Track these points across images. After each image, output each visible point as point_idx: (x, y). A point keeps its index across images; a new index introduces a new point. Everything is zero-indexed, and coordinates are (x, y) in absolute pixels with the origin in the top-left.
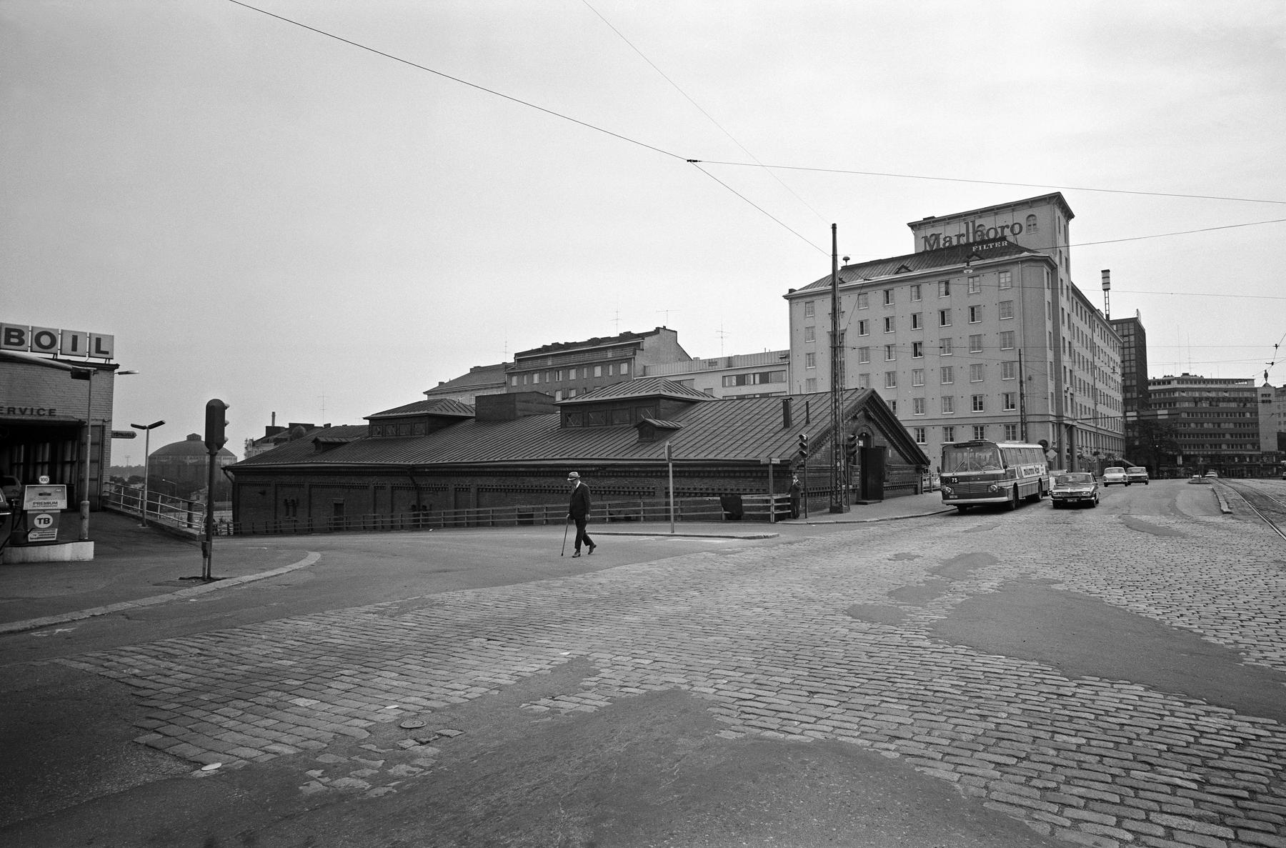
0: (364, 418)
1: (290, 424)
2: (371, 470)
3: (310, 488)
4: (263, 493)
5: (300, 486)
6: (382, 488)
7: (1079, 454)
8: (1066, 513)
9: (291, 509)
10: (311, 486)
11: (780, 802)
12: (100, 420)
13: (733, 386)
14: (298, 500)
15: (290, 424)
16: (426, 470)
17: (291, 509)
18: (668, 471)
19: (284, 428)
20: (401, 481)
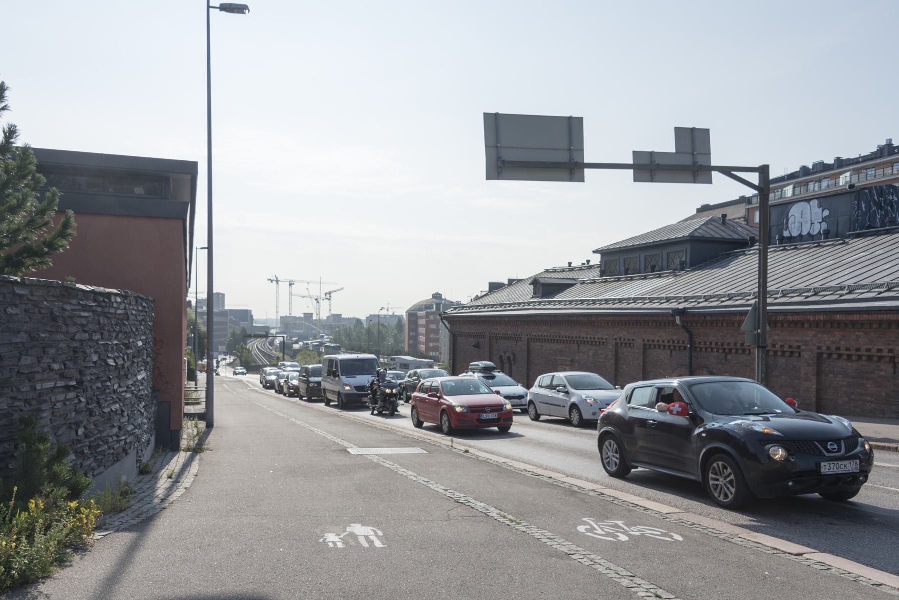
0: (594, 252)
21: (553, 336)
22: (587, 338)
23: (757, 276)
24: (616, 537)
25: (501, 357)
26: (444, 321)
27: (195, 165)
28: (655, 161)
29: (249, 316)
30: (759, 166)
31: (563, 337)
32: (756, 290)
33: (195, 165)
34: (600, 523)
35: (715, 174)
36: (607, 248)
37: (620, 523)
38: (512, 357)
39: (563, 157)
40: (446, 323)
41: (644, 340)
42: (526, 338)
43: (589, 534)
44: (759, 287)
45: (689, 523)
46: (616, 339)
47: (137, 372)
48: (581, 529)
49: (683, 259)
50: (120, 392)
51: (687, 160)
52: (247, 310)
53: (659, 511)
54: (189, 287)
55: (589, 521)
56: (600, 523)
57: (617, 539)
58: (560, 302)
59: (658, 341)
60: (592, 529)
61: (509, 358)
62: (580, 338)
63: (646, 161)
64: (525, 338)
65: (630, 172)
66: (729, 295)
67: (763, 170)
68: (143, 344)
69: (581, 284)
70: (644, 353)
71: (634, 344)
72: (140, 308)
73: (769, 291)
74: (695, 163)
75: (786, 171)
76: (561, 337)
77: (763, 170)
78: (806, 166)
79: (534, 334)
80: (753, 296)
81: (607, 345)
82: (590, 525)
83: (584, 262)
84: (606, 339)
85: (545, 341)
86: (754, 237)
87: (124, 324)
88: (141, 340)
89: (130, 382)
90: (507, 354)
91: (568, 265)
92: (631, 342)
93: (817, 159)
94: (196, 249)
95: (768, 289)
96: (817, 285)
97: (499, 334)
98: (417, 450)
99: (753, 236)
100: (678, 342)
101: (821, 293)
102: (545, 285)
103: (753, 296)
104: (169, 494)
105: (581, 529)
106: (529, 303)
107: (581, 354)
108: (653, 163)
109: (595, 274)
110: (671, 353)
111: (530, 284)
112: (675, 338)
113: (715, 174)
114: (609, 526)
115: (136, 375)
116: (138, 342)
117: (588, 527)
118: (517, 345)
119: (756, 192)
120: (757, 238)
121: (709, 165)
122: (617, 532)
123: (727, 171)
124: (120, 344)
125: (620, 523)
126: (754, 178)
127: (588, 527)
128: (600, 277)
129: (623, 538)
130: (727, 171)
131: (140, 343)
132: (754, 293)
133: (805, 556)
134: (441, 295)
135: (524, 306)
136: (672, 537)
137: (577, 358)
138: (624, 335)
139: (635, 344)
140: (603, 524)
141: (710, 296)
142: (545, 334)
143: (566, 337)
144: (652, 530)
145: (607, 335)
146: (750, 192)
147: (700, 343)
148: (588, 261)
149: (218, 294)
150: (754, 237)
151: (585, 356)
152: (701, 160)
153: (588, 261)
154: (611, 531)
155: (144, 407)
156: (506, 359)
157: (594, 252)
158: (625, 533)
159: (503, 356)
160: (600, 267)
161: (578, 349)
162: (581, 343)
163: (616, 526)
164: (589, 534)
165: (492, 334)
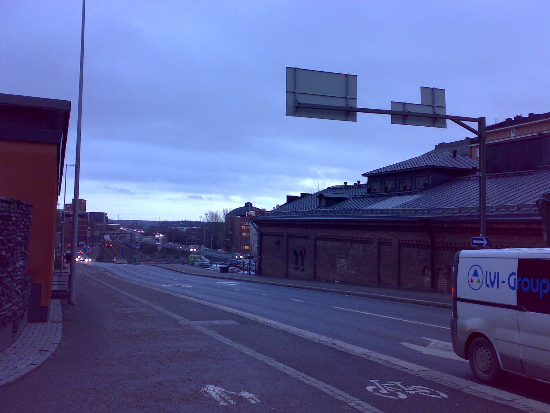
0: (363, 175)
1: (301, 194)
2: (469, 225)
3: (315, 240)
4: (278, 243)
5: (307, 237)
6: (388, 244)
7: (481, 173)
8: (391, 301)
9: (300, 258)
10: (401, 245)
11: (145, 388)
12: (371, 187)
13: (30, 225)
14: (305, 250)
15: (301, 194)
16: (445, 225)
17: (300, 258)
18: (79, 228)
19: (298, 197)
20: (411, 237)
21: (334, 236)
22: (358, 238)
23: (479, 195)
24: (397, 395)
25: (295, 251)
26: (253, 223)
27: (69, 103)
28: (406, 110)
29: (105, 218)
30: (479, 118)
31: (340, 236)
32: (478, 205)
33: (69, 103)
34: (383, 385)
35: (448, 121)
36: (372, 173)
37: (398, 384)
38: (303, 251)
39: (341, 103)
40: (255, 225)
41: (399, 240)
42: (314, 237)
43: (376, 393)
44: (480, 203)
45: (434, 378)
46: (379, 239)
47: (16, 261)
48: (370, 388)
49: (427, 182)
50: (2, 277)
51: (428, 111)
52: (103, 213)
53: (412, 369)
54: (59, 195)
55: (375, 382)
56: (383, 385)
57: (398, 398)
58: (338, 211)
59: (409, 241)
60: (378, 390)
61: (301, 251)
62: (352, 237)
63: (399, 109)
64: (313, 237)
65: (389, 117)
66: (459, 208)
67: (481, 121)
68: (22, 239)
69: (353, 198)
70: (399, 249)
71: (391, 243)
72: (21, 212)
73: (487, 207)
74: (434, 112)
75: (496, 122)
76: (339, 237)
77: (481, 121)
78: (509, 119)
79: (320, 234)
80: (476, 210)
81: (372, 244)
82: (376, 386)
83: (355, 182)
84: (372, 238)
85: (328, 240)
86: (476, 168)
87: (8, 224)
88: (20, 236)
89: (10, 269)
90: (300, 249)
91: (344, 185)
92: (389, 241)
93: (517, 114)
94: (66, 166)
95: (487, 205)
96: (519, 203)
97: (294, 234)
98: (232, 322)
99: (476, 166)
100: (424, 242)
101: (522, 209)
102: (327, 199)
103: (476, 210)
104: (13, 348)
105: (370, 388)
106: (316, 212)
107: (353, 249)
108: (405, 111)
109: (364, 192)
110: (418, 250)
111: (317, 198)
112: (421, 239)
113: (448, 121)
114: (392, 386)
115: (15, 264)
116: (18, 238)
117: (374, 387)
118: (307, 242)
119: (476, 136)
120: (478, 168)
121: (445, 115)
122: (397, 391)
123: (458, 120)
124: (4, 240)
125: (398, 384)
126: (475, 126)
127: (374, 387)
128: (368, 194)
129: (403, 396)
130: (458, 120)
131: (20, 239)
132: (477, 207)
133: (517, 401)
134: (251, 204)
135: (312, 214)
136: (439, 395)
137: (350, 252)
138: (385, 236)
139: (392, 243)
140: (386, 385)
141: (446, 209)
142: (328, 235)
143: (343, 237)
144: (423, 389)
145: (373, 236)
146: (473, 136)
147: (439, 243)
148: (359, 182)
149: (81, 200)
150: (476, 168)
151: (357, 252)
152: (439, 111)
153: (359, 182)
154: (392, 391)
155: (20, 288)
156: (299, 252)
157: (363, 175)
158: (403, 392)
159: (297, 250)
160: (367, 186)
161: (352, 246)
162: (354, 242)
163: (396, 386)
164: (376, 393)
165: (289, 233)
